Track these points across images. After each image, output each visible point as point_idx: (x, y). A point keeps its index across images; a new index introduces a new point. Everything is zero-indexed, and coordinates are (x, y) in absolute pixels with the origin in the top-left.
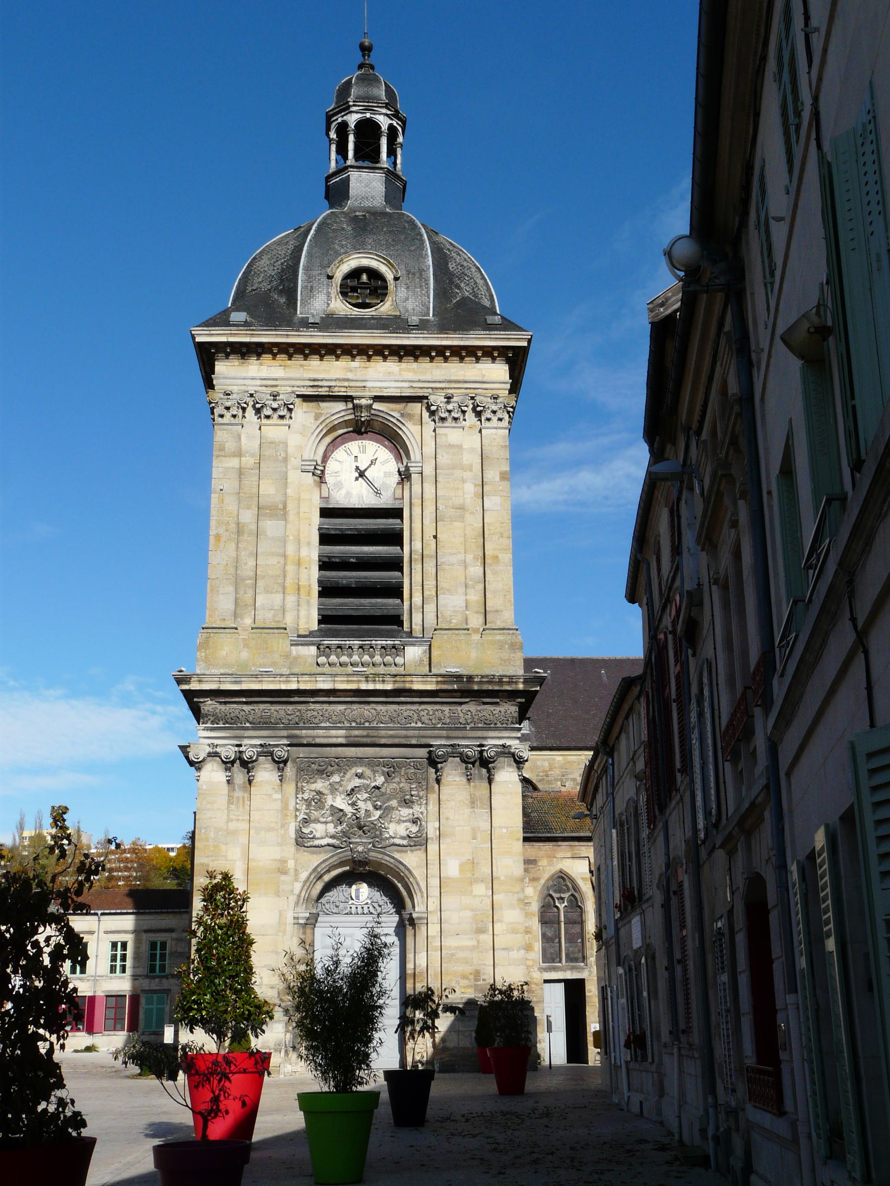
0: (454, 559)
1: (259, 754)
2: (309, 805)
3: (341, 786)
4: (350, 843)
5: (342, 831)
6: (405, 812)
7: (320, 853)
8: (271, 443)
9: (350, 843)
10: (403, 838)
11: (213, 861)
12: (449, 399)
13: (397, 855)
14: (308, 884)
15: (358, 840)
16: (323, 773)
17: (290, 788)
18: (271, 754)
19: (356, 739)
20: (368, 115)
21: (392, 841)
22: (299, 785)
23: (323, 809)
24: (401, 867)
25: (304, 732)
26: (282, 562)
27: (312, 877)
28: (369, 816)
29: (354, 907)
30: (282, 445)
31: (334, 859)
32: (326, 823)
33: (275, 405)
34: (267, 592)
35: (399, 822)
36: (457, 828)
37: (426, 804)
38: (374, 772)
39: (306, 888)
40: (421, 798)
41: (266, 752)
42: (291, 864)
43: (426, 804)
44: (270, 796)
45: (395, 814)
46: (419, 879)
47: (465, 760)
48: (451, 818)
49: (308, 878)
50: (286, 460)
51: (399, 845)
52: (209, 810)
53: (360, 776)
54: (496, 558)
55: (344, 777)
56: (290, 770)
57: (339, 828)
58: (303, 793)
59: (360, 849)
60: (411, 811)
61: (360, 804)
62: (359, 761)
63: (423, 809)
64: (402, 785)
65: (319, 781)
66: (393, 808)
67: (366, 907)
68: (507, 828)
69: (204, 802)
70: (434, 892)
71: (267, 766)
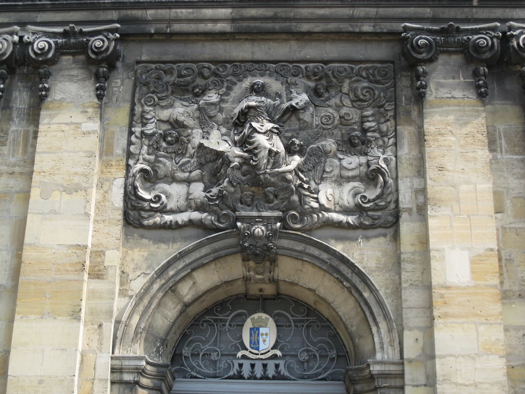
1: (61, 50)
2: (155, 149)
3: (221, 110)
4: (238, 219)
5: (221, 196)
6: (352, 162)
7: (174, 241)
9: (238, 219)
10: (346, 211)
13: (338, 247)
14: (146, 301)
16: (187, 90)
17: (120, 116)
18: (83, 48)
19: (252, 24)
22: (138, 109)
23: (183, 155)
27: (156, 286)
28: (276, 164)
29: (247, 365)
31: (204, 251)
32: (188, 182)
35: (341, 180)
37: (395, 144)
38: (289, 86)
39: (141, 308)
40: (383, 135)
41: (73, 45)
42: (113, 258)
43: (395, 144)
45: (332, 165)
46: (382, 293)
47: (470, 54)
48: (449, 167)
49: (146, 290)
51: (339, 225)
53: (257, 90)
55: (227, 94)
56: (121, 84)
57: (215, 190)
58: (144, 125)
59: (259, 230)
60: (363, 160)
61: (261, 140)
62: (258, 65)
63: (389, 154)
64: (344, 111)
65: (178, 103)
66: (326, 154)
67: (271, 365)
70: (413, 318)
71: (75, 72)
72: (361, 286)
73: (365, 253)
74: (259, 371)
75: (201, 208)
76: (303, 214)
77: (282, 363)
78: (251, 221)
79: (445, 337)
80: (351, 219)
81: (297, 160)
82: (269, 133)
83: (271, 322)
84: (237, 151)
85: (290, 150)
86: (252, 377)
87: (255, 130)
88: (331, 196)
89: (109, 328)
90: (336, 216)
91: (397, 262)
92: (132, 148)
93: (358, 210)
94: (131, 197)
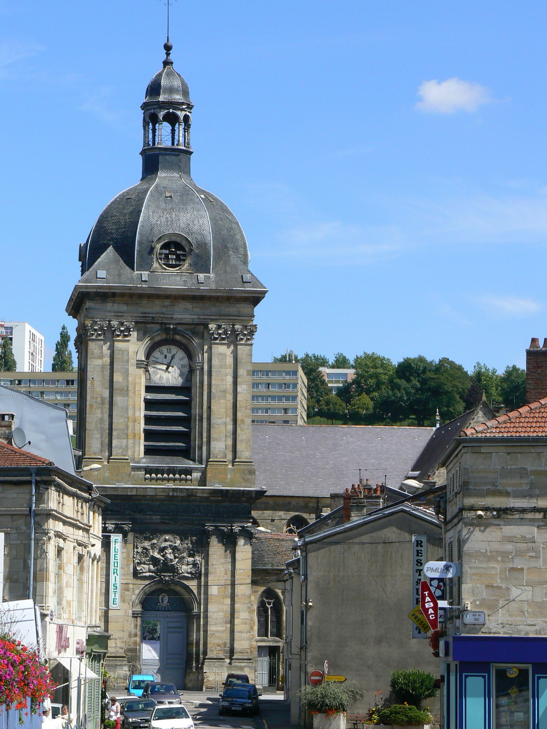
0: (219, 421)
6: (191, 559)
8: (120, 350)
10: (188, 573)
12: (219, 327)
13: (185, 582)
20: (171, 111)
26: (127, 421)
30: (126, 352)
33: (122, 329)
34: (118, 438)
35: (188, 565)
38: (175, 538)
50: (128, 361)
54: (243, 421)
59: (167, 578)
60: (193, 559)
61: (168, 556)
73: (192, 585)
74: (163, 609)
76: (178, 574)
78: (165, 576)
79: (211, 607)
80: (190, 575)
81: (177, 560)
82: (170, 553)
84: (163, 559)
85: (175, 557)
86: (162, 610)
87: (166, 553)
88: (185, 569)
89: (131, 603)
90: (186, 575)
91: (199, 586)
93: (191, 573)
94: (135, 569)
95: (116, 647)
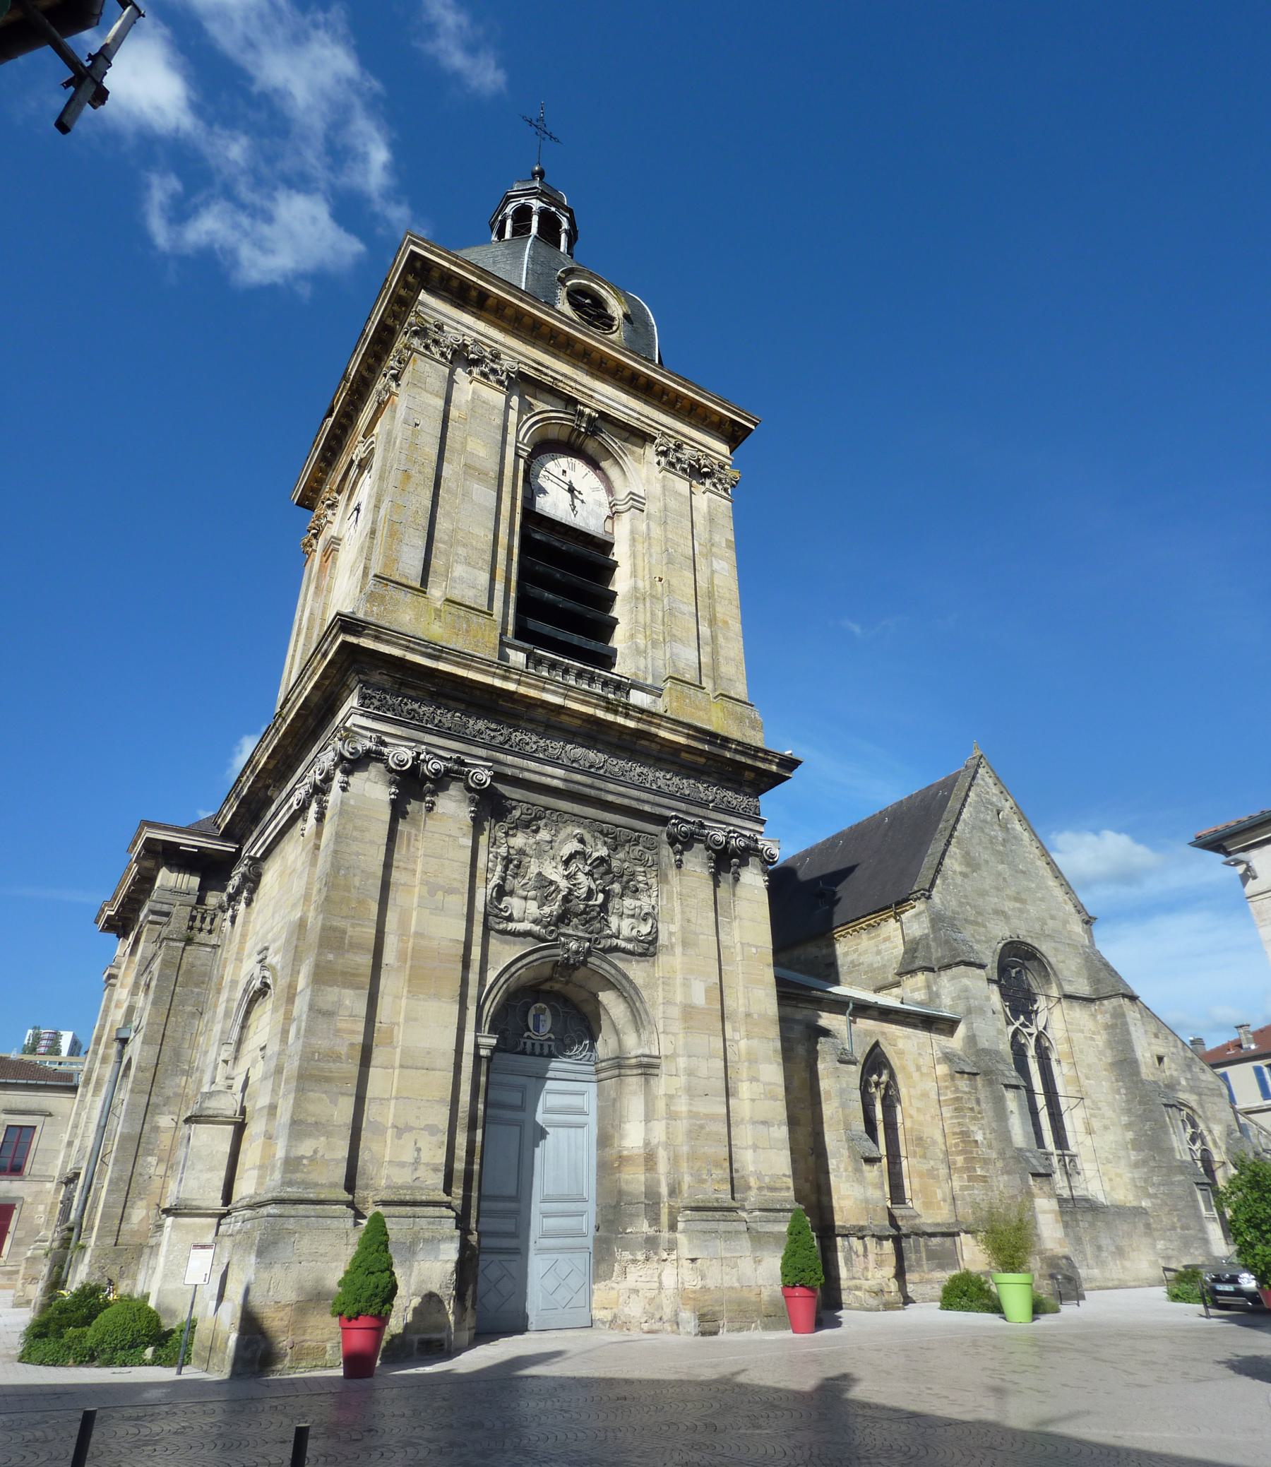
10: (629, 940)
11: (353, 926)
13: (620, 965)
15: (571, 932)
21: (615, 941)
24: (624, 982)
25: (509, 757)
27: (502, 980)
29: (529, 1042)
32: (525, 898)
36: (702, 937)
44: (455, 838)
48: (693, 920)
51: (624, 951)
52: (355, 839)
60: (638, 903)
62: (577, 819)
68: (757, 947)
69: (350, 826)
72: (635, 997)
73: (636, 971)
74: (537, 1051)
75: (535, 922)
77: (552, 1043)
83: (548, 1012)
86: (533, 1054)
90: (623, 944)
92: (490, 864)
95: (417, 1162)
